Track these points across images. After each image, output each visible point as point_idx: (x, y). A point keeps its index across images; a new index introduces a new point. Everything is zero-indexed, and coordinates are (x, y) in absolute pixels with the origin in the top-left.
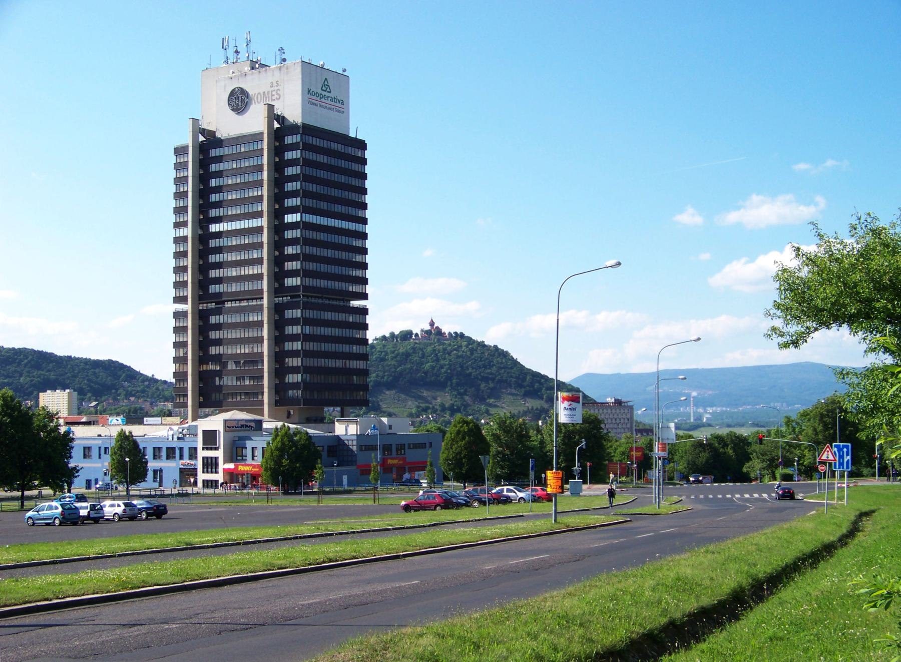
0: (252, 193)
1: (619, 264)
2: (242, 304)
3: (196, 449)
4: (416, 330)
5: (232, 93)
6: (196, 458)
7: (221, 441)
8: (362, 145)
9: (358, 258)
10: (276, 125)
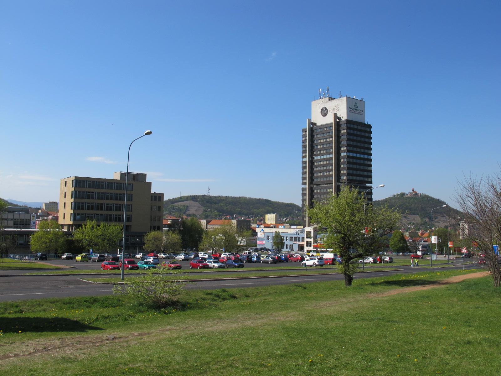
3: (304, 238)
4: (407, 192)
5: (322, 110)
6: (304, 241)
7: (312, 235)
9: (368, 168)
10: (337, 120)
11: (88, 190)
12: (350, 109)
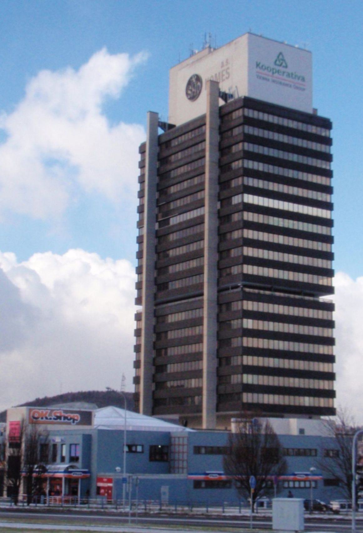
0: (193, 247)
2: (204, 509)
5: (190, 83)
11: (135, 518)
12: (257, 67)
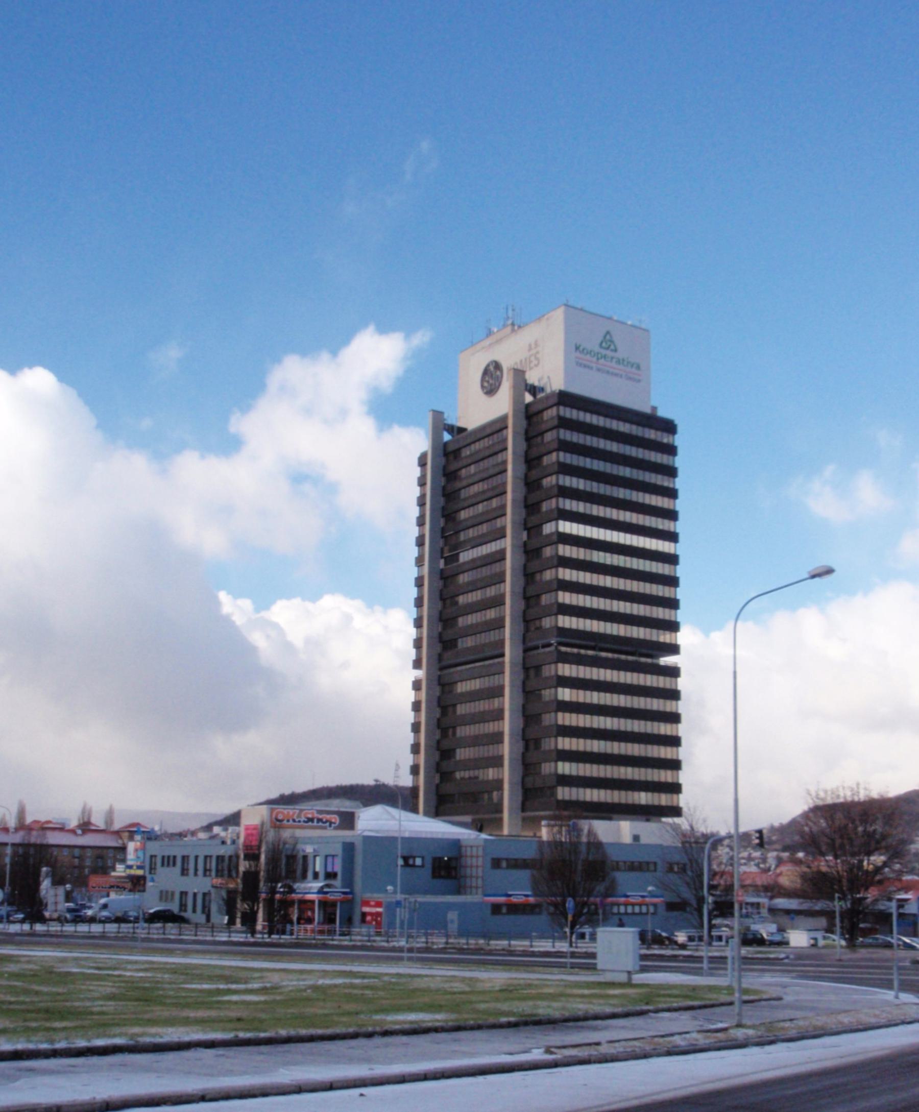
1: (829, 571)
5: (486, 372)
8: (669, 427)
12: (577, 351)
